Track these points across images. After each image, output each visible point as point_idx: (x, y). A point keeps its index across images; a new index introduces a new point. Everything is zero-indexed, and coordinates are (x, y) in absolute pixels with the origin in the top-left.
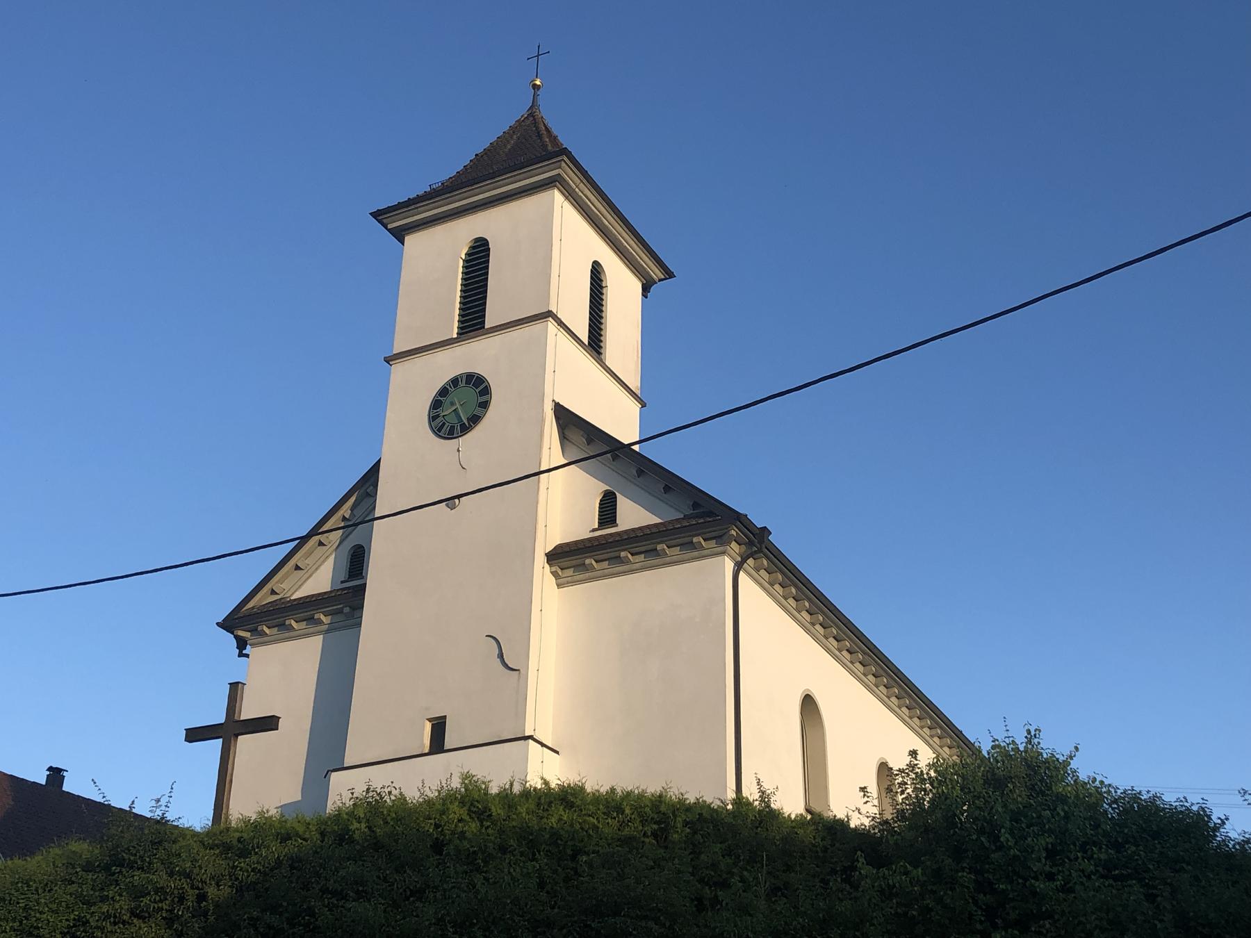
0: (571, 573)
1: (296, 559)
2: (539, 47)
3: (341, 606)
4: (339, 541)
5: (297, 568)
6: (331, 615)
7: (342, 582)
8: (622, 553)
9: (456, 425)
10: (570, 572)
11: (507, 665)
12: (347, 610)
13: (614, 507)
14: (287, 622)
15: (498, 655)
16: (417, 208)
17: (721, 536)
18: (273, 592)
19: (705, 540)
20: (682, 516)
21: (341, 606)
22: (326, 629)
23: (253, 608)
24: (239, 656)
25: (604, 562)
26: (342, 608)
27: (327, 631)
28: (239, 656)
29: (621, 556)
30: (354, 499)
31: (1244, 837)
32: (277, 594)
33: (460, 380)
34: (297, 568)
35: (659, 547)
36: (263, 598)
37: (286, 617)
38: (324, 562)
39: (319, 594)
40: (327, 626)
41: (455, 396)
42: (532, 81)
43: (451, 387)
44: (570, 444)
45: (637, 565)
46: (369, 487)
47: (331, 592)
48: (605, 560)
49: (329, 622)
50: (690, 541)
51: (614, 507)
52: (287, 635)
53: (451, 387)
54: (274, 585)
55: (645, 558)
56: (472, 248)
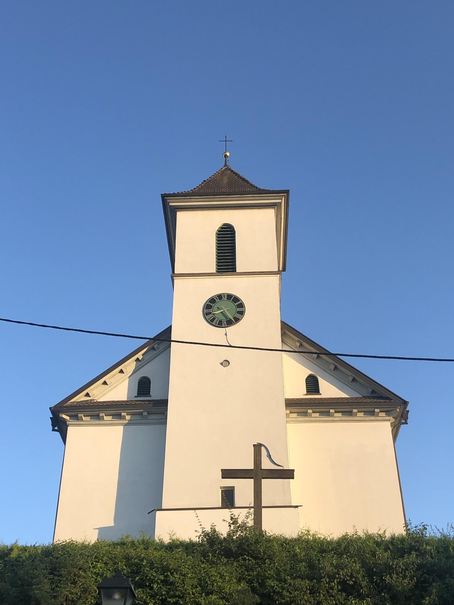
0: (296, 416)
1: (106, 378)
2: (226, 137)
3: (142, 411)
4: (132, 372)
5: (105, 383)
6: (130, 415)
7: (136, 397)
8: (331, 410)
9: (223, 321)
10: (295, 415)
11: (274, 462)
12: (145, 414)
13: (149, 390)
14: (79, 415)
15: (267, 455)
16: (191, 199)
17: (390, 411)
18: (87, 395)
19: (84, 416)
20: (361, 396)
21: (142, 411)
22: (126, 423)
23: (73, 402)
24: (52, 431)
25: (110, 416)
26: (142, 412)
27: (126, 425)
28: (52, 431)
29: (122, 415)
30: (146, 350)
31: (14, 551)
32: (90, 397)
33: (223, 296)
34: (105, 383)
35: (123, 414)
36: (81, 398)
37: (100, 411)
38: (120, 383)
39: (118, 401)
40: (128, 421)
41: (219, 303)
42: (224, 153)
43: (224, 297)
44: (285, 345)
45: (338, 419)
46: (155, 344)
47: (126, 401)
48: (89, 416)
49: (129, 419)
50: (119, 413)
51: (149, 390)
52: (98, 422)
53: (224, 297)
54: (89, 391)
55: (90, 419)
56: (222, 228)
